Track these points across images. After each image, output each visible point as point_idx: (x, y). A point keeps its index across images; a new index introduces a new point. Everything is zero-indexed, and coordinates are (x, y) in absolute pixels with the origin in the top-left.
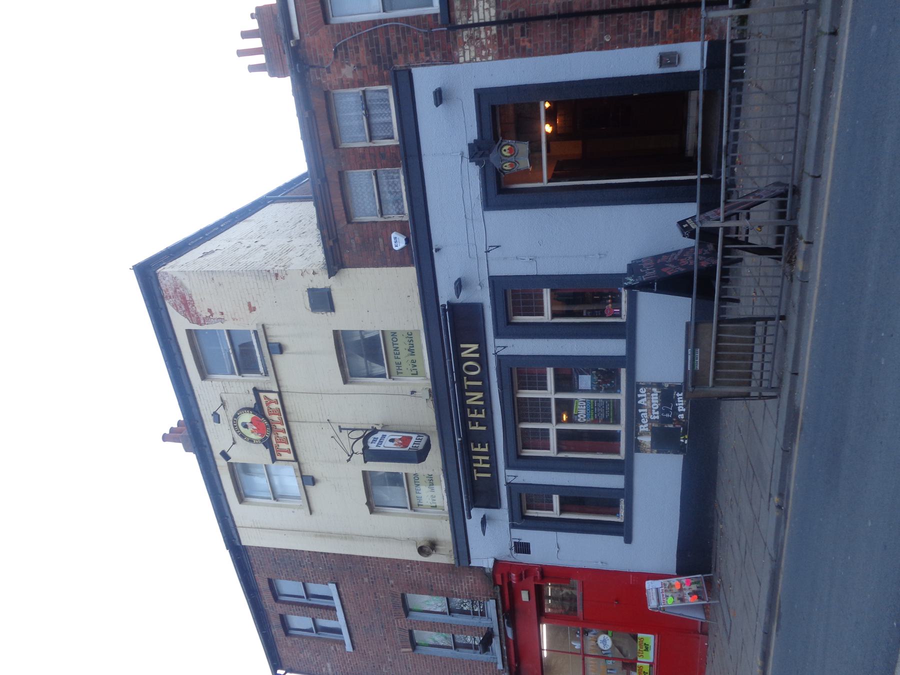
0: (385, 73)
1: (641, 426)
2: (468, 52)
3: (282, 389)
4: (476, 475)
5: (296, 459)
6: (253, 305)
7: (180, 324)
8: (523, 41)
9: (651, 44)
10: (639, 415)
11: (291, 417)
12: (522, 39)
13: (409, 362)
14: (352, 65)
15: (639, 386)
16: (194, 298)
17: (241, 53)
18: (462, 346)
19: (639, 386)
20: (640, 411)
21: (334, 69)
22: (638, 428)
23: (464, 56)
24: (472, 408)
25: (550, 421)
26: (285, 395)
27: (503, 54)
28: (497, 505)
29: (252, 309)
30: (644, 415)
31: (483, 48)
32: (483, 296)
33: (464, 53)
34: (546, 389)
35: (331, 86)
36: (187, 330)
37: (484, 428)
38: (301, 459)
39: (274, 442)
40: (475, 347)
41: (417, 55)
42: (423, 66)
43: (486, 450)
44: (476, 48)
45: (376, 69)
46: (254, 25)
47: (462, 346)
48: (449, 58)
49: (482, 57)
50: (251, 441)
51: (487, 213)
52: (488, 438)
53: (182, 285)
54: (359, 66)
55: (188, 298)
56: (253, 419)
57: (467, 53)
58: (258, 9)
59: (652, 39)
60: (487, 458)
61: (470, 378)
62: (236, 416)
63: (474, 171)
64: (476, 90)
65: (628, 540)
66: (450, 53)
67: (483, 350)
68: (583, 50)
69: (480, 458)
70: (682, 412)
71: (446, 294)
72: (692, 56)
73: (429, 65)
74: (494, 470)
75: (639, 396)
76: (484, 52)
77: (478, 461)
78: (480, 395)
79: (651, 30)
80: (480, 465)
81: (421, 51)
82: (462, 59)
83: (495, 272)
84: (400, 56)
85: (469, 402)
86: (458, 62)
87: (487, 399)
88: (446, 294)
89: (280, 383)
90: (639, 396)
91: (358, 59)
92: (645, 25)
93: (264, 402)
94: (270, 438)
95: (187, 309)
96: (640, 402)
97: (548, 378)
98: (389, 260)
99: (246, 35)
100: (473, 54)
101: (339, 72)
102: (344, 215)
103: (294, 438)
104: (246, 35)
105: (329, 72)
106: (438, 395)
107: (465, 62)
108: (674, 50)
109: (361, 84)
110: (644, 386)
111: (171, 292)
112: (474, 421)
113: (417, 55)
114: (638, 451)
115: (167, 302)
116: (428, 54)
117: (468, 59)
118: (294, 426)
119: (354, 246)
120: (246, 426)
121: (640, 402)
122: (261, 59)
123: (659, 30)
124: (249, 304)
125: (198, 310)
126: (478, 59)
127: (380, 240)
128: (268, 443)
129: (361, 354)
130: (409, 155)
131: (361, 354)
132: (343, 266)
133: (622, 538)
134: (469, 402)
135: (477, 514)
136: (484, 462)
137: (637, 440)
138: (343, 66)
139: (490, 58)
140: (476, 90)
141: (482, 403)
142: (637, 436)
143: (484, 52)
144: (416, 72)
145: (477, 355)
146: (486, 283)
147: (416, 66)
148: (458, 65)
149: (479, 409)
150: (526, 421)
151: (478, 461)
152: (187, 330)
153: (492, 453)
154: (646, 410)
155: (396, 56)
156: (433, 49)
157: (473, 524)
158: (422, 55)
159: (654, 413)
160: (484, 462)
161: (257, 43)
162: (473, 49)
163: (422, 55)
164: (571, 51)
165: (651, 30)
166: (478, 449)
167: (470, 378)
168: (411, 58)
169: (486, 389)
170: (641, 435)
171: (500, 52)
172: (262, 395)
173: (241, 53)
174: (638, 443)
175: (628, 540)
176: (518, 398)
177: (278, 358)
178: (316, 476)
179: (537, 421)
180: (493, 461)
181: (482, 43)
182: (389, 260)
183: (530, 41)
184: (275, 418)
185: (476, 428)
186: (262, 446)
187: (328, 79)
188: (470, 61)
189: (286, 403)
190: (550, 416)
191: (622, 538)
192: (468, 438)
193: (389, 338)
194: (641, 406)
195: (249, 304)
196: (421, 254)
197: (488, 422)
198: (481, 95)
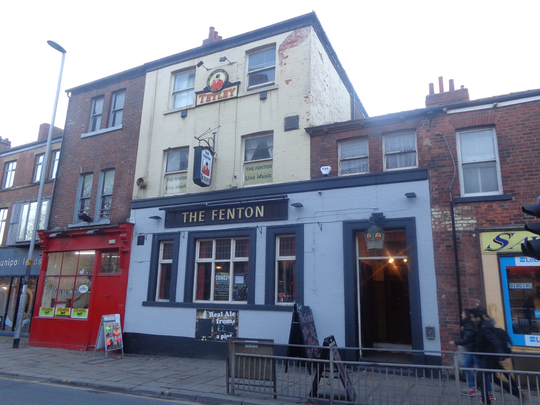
1: (212, 313)
2: (437, 214)
3: (239, 99)
4: (185, 214)
5: (197, 106)
6: (289, 82)
7: (279, 39)
12: (444, 245)
13: (253, 175)
14: (431, 145)
15: (236, 312)
16: (295, 48)
17: (441, 79)
18: (263, 207)
20: (222, 312)
21: (429, 134)
23: (435, 211)
24: (225, 212)
25: (216, 258)
26: (234, 101)
27: (436, 234)
28: (167, 226)
29: (287, 82)
31: (440, 223)
32: (292, 220)
33: (437, 211)
35: (418, 132)
37: (213, 219)
38: (197, 109)
40: (262, 214)
41: (436, 183)
42: (430, 187)
44: (440, 218)
46: (457, 87)
47: (263, 207)
49: (434, 222)
50: (209, 80)
53: (302, 41)
54: (430, 149)
56: (222, 81)
57: (437, 213)
58: (466, 90)
59: (443, 323)
60: (195, 220)
62: (224, 71)
64: (414, 218)
65: (144, 304)
67: (260, 219)
69: (195, 217)
70: (220, 337)
71: (293, 198)
74: (188, 224)
75: (231, 312)
76: (437, 223)
77: (193, 215)
78: (233, 217)
79: (448, 323)
80: (191, 216)
82: (433, 210)
85: (229, 210)
86: (431, 207)
87: (230, 221)
90: (231, 312)
91: (434, 148)
92: (452, 319)
93: (232, 88)
95: (288, 43)
96: (227, 312)
98: (315, 164)
99: (451, 82)
100: (436, 217)
101: (427, 137)
102: (342, 138)
103: (209, 106)
104: (451, 82)
106: (233, 192)
107: (432, 212)
110: (236, 315)
111: (298, 34)
112: (218, 213)
113: (436, 183)
114: (198, 311)
116: (436, 190)
117: (433, 213)
119: (323, 144)
120: (217, 77)
121: (227, 312)
122: (437, 91)
124: (290, 80)
125: (287, 50)
126: (433, 220)
127: (327, 159)
128: (207, 90)
129: (259, 147)
130: (376, 177)
132: (312, 137)
134: (229, 210)
135: (162, 214)
136: (193, 219)
137: (204, 310)
138: (431, 139)
139: (434, 227)
140: (414, 218)
143: (437, 223)
145: (257, 216)
146: (300, 222)
147: (429, 183)
149: (225, 216)
150: (217, 244)
151: (193, 215)
153: (198, 224)
155: (436, 171)
156: (439, 193)
157: (156, 211)
158: (436, 186)
159: (220, 321)
162: (439, 216)
164: (436, 274)
166: (200, 215)
167: (243, 211)
168: (434, 180)
169: (236, 220)
170: (207, 313)
171: (437, 233)
172: (236, 87)
173: (441, 79)
174: (202, 311)
177: (258, 97)
178: (187, 118)
180: (193, 224)
181: (442, 222)
182: (315, 164)
183: (443, 250)
184: (222, 94)
185: (213, 214)
188: (432, 215)
190: (220, 259)
191: (145, 299)
192: (207, 210)
194: (224, 313)
195: (290, 80)
196: (318, 184)
197: (217, 222)
198: (411, 221)
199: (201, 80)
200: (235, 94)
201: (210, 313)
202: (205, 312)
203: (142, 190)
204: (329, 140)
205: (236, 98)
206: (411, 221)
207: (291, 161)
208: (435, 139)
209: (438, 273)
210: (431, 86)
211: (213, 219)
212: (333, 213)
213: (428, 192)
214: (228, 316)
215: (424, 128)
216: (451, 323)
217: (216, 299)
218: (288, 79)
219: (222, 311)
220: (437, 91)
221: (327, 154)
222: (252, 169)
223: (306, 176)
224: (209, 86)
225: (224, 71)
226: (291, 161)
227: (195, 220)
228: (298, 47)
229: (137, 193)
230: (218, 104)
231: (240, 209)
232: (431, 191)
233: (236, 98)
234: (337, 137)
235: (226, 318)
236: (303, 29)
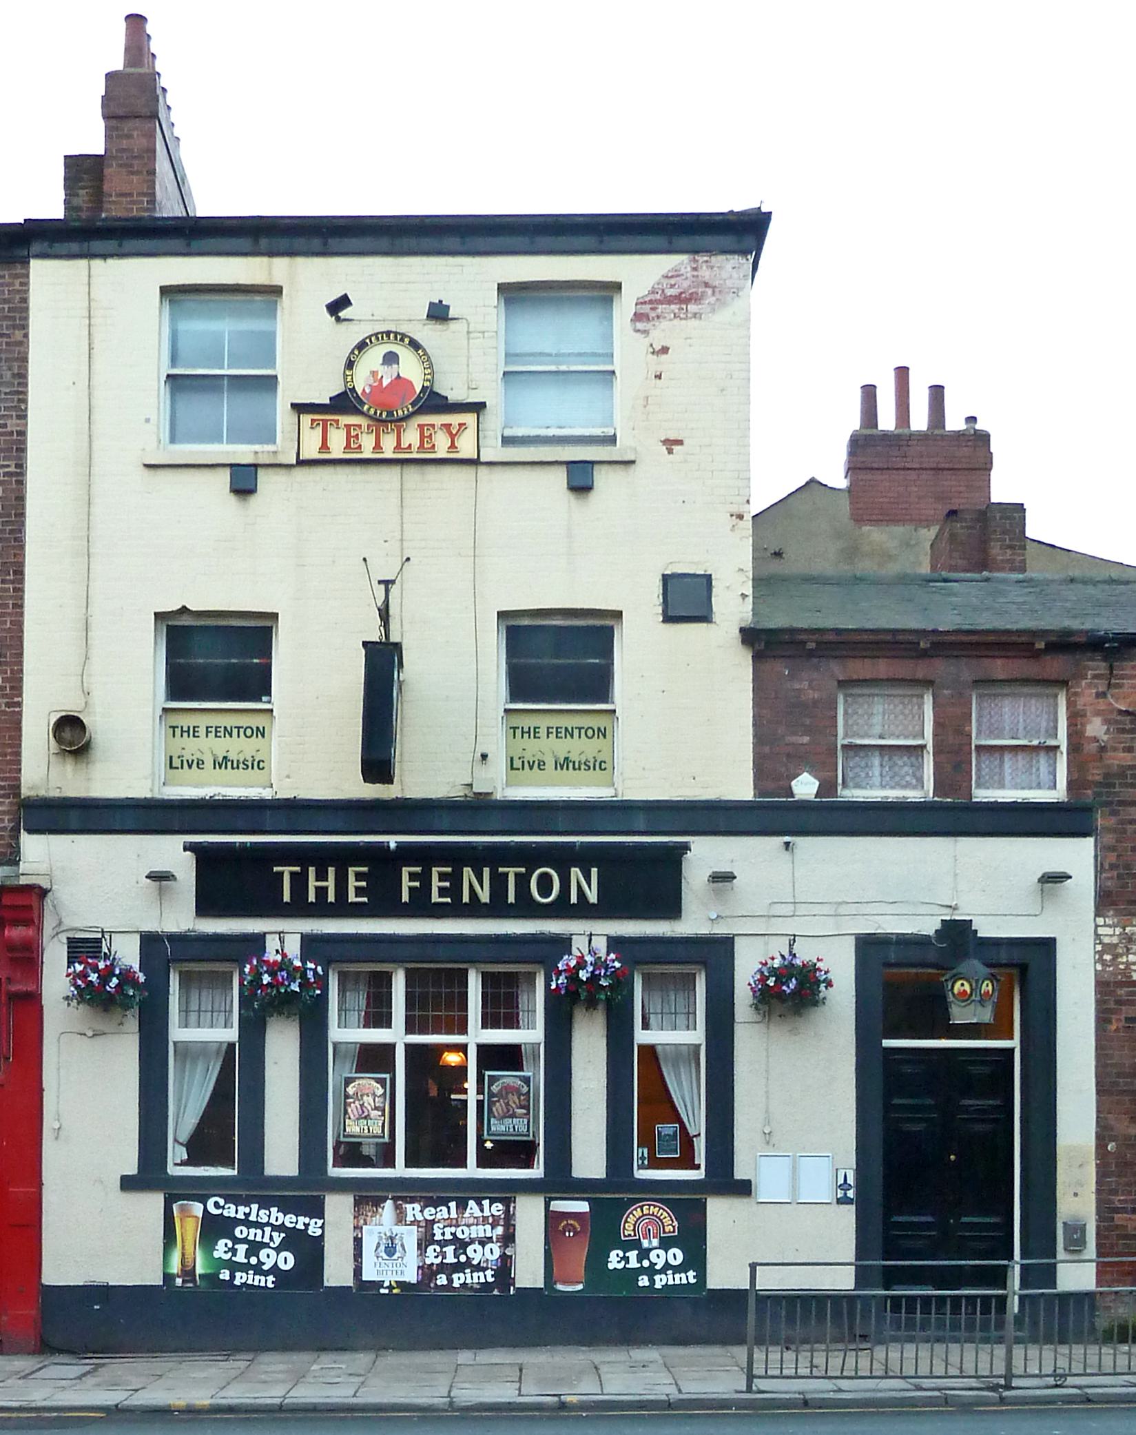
0: (1089, 792)
1: (417, 1206)
2: (1111, 933)
3: (483, 471)
4: (287, 870)
5: (301, 463)
6: (676, 448)
7: (638, 273)
8: (1119, 1020)
9: (1098, 1212)
10: (444, 1202)
11: (412, 473)
12: (1122, 1017)
13: (539, 756)
14: (1105, 738)
15: (507, 1202)
16: (693, 323)
17: (902, 373)
18: (594, 871)
19: (507, 1202)
20: (453, 1205)
21: (1102, 705)
22: (412, 1200)
23: (1105, 925)
24: (456, 879)
25: (410, 1029)
26: (467, 473)
27: (1103, 986)
28: (205, 907)
29: (671, 444)
30: (443, 1212)
31: (1116, 956)
32: (694, 921)
33: (1109, 926)
34: (484, 1026)
35: (1076, 694)
36: (617, 287)
37: (405, 897)
38: (301, 474)
39: (346, 420)
40: (593, 897)
41: (1112, 849)
42: (1096, 857)
43: (352, 898)
44: (1116, 945)
45: (1097, 778)
46: (954, 422)
47: (594, 871)
48: (1105, 901)
49: (1101, 953)
50: (350, 365)
51: (850, 944)
52: (384, 902)
53: (721, 303)
54: (1103, 749)
55: (692, 308)
56: (410, 384)
57: (1109, 931)
58: (983, 439)
59: (1105, 1210)
60: (331, 898)
61: (522, 881)
62: (415, 345)
63: (928, 926)
64: (1054, 940)
65: (128, 1184)
66: (1114, 903)
67: (584, 910)
68: (1098, 1111)
69: (330, 884)
70: (450, 1281)
71: (705, 855)
72: (1077, 1275)
73: (1096, 867)
74: (299, 908)
75: (486, 1203)
76: (1107, 957)
77: (322, 876)
78: (485, 896)
79: (1117, 1210)
80: (312, 884)
81: (1118, 856)
82: (1100, 921)
83: (739, 944)
84: (1112, 821)
85: (468, 872)
86: (1097, 915)
87: (475, 910)
88: (705, 855)
89: (498, 469)
90: (486, 1203)
91: (1115, 749)
92: (1125, 1201)
93: (454, 419)
94: (359, 412)
95: (669, 300)
96: (472, 1203)
97: (435, 1036)
98: (767, 749)
99: (937, 393)
100: (1106, 940)
101: (1098, 713)
102: (855, 677)
103: (358, 469)
104: (937, 393)
105: (1098, 695)
106: (476, 809)
107: (1097, 926)
108: (1088, 1245)
109: (1075, 746)
110: (507, 1211)
111: (705, 273)
112: (425, 878)
113: (1112, 849)
114: (357, 1203)
115: (684, 258)
116: (1113, 867)
117: (1100, 931)
118: (391, 475)
119: (797, 686)
120: (391, 358)
121: (472, 1203)
122: (887, 421)
123: (1117, 1222)
124: (679, 442)
125: (664, 324)
126: (1099, 948)
127: (806, 739)
128: (344, 403)
129: (559, 660)
130: (955, 816)
131: (559, 660)
132: (758, 658)
133: (132, 1170)
134: (468, 872)
135: (184, 867)
136: (322, 892)
137: (385, 1199)
138: (1107, 722)
139: (1099, 967)
140: (1054, 940)
141: (466, 899)
142: (394, 1199)
143: (1107, 957)
144: (1090, 841)
145: (574, 899)
146: (721, 930)
147: (1096, 846)
148: (1092, 915)
149: (454, 890)
150: (408, 984)
151: (322, 876)
152: (617, 287)
153: (342, 909)
154: (454, 1215)
155: (1114, 813)
156: (1119, 876)
157: (172, 852)
158: (1112, 857)
159: (448, 1230)
160: (322, 892)
161: (919, 421)
162: (1115, 940)
163: (1112, 857)
164: (1100, 1091)
165: (1117, 1210)
166: (352, 883)
167: (522, 881)
168: (1109, 839)
169: (498, 908)
170: (397, 1207)
171: (1107, 984)
172: (470, 419)
173: (902, 373)
174: (378, 1202)
175: (128, 1184)
176: (467, 970)
177: (559, 477)
178: (254, 500)
179: (410, 1004)
180: (322, 909)
181: (1121, 955)
182: (767, 749)
183: (1117, 1030)
184: (411, 436)
185: (406, 884)
186: (338, 389)
187: (1087, 692)
188: (1097, 935)
189: (448, 471)
190: (423, 1031)
191: (132, 1170)
192: (384, 864)
193: (595, 722)
194: (462, 1206)
195: (679, 442)
196: (769, 816)
197: (421, 907)
198: (1047, 946)
199: (308, 357)
200: (466, 448)
201: (409, 1207)
202: (389, 1204)
203: (70, 760)
204: (815, 675)
205: (475, 462)
206: (1047, 946)
207: (681, 721)
208: (1117, 722)
209: (1103, 1089)
210: (869, 393)
211: (405, 897)
212: (826, 910)
213: (28, 570)
214: (478, 1213)
215: (1089, 686)
216: (1124, 1210)
217: (481, 1163)
218: (673, 436)
219: (452, 1199)
220: (887, 421)
221: (808, 722)
222: (534, 733)
223: (743, 790)
224: (353, 390)
225: (415, 345)
226: (681, 721)
227: (331, 898)
228: (702, 323)
229: (41, 770)
230: (396, 470)
231: (511, 871)
232: (1099, 869)
233: (475, 462)
234: (838, 669)
235: (471, 1221)
236: (721, 258)
